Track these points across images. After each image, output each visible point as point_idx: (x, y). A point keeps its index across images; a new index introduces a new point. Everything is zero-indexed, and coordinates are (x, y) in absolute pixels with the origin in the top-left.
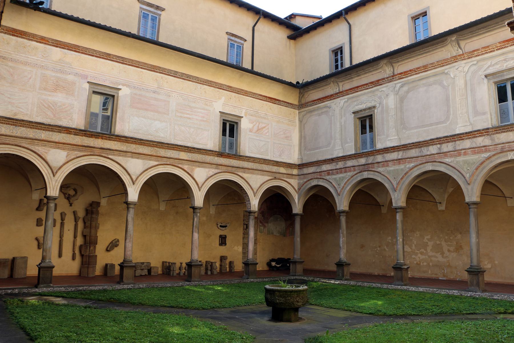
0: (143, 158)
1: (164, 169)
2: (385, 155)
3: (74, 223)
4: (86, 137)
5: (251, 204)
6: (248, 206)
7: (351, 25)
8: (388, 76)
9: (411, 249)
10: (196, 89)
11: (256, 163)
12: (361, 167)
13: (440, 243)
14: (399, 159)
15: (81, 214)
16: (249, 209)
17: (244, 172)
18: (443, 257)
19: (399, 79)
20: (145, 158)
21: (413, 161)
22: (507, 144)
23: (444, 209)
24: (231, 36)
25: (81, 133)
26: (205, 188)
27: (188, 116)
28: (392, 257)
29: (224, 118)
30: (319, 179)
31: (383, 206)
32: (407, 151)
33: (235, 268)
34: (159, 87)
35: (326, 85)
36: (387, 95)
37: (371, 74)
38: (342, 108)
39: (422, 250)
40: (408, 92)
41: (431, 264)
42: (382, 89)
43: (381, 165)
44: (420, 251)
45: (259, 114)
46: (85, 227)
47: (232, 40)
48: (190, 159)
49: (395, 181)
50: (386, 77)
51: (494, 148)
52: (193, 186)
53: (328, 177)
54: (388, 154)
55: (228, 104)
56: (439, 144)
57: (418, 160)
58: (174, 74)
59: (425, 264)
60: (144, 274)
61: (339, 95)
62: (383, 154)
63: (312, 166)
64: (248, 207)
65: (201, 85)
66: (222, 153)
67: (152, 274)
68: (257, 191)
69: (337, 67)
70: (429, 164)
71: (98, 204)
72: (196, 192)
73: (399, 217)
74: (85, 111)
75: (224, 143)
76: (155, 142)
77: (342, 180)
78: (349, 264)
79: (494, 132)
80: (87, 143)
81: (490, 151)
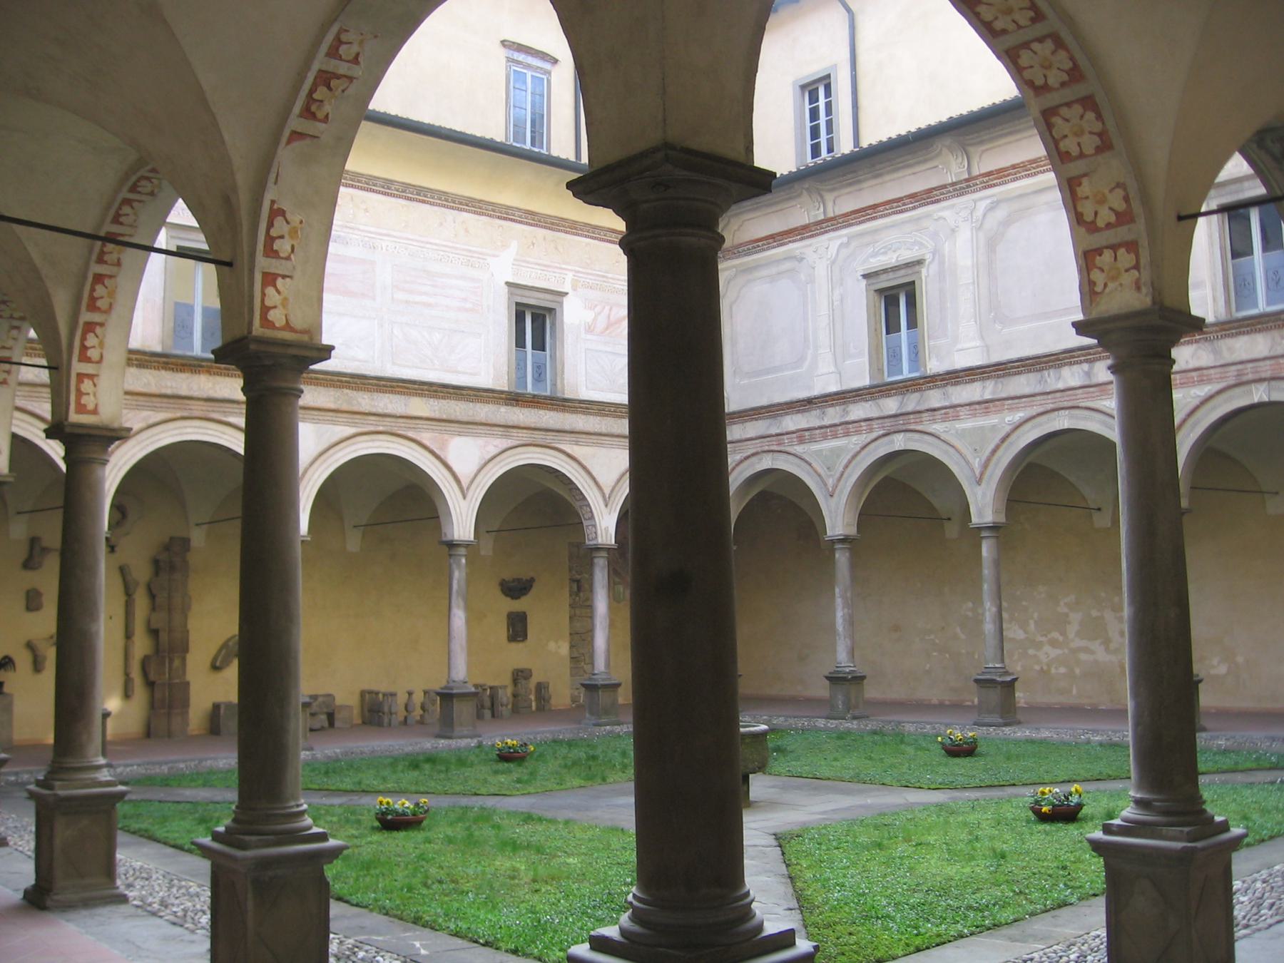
0: (316, 417)
1: (370, 444)
2: (950, 389)
3: (123, 599)
4: (168, 372)
5: (598, 527)
6: (589, 532)
7: (853, 14)
8: (954, 180)
9: (1026, 632)
10: (441, 224)
11: (607, 415)
12: (886, 420)
13: (1099, 614)
14: (987, 402)
15: (142, 573)
16: (593, 539)
17: (577, 443)
18: (1107, 650)
19: (985, 188)
20: (320, 418)
21: (1023, 405)
22: (1251, 365)
23: (1109, 525)
24: (515, 50)
25: (155, 362)
26: (478, 491)
27: (424, 299)
28: (976, 657)
29: (519, 300)
30: (775, 454)
31: (949, 519)
32: (1005, 380)
33: (553, 701)
34: (348, 225)
35: (790, 198)
36: (953, 231)
37: (909, 171)
38: (833, 262)
39: (1055, 635)
40: (1007, 223)
41: (1077, 671)
42: (941, 214)
43: (939, 417)
44: (1049, 636)
45: (608, 282)
46: (154, 608)
47: (518, 63)
48: (437, 415)
49: (975, 458)
50: (950, 181)
51: (1221, 373)
52: (447, 485)
53: (799, 449)
54: (958, 388)
55: (528, 259)
56: (1087, 361)
57: (1035, 403)
58: (383, 187)
59: (1062, 670)
60: (317, 726)
61: (824, 225)
62: (945, 386)
63: (756, 419)
64: (590, 536)
65: (455, 212)
66: (517, 394)
67: (337, 724)
68: (612, 491)
69: (816, 151)
70: (1062, 412)
71: (185, 543)
72: (456, 502)
73: (987, 549)
74: (161, 301)
75: (520, 365)
76: (345, 375)
77: (838, 456)
78: (863, 678)
79: (1219, 334)
80: (171, 387)
81: (1209, 381)
